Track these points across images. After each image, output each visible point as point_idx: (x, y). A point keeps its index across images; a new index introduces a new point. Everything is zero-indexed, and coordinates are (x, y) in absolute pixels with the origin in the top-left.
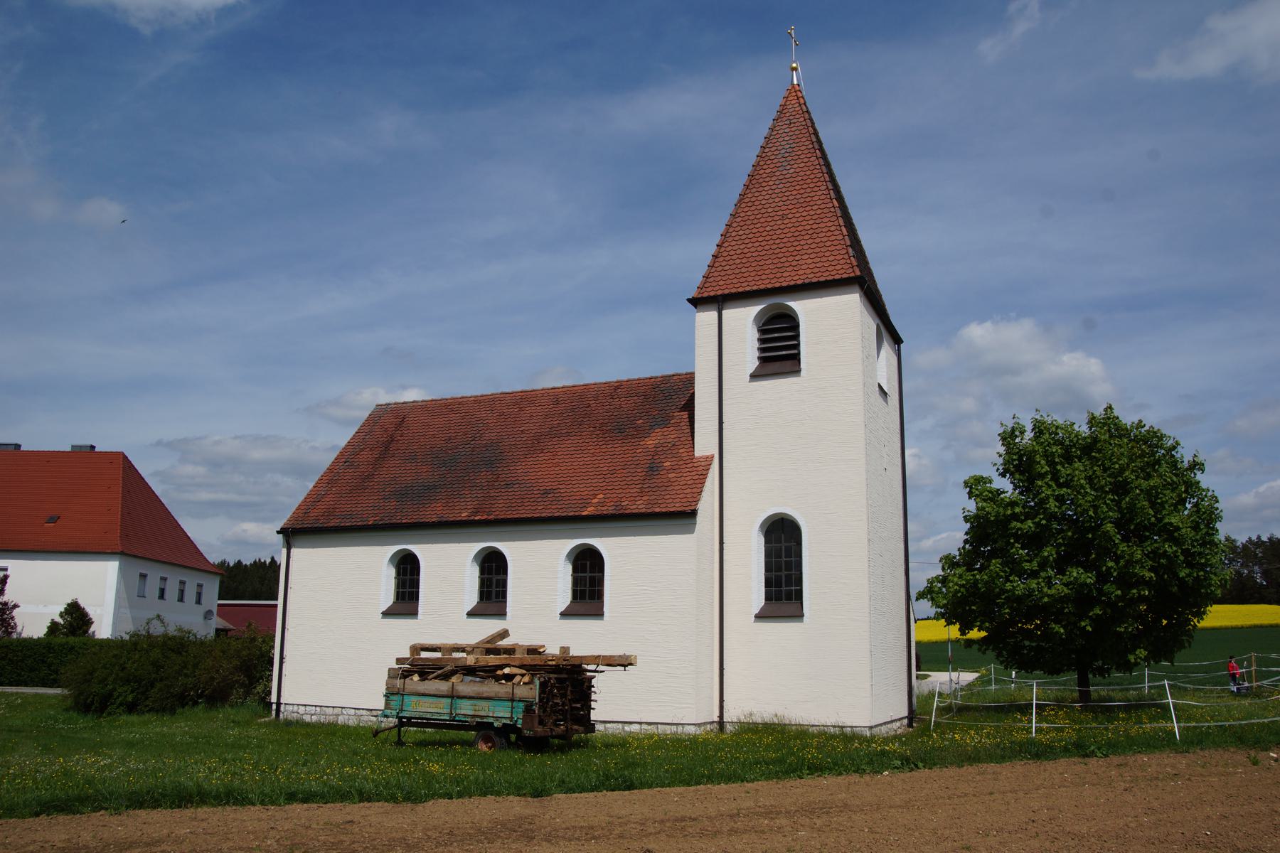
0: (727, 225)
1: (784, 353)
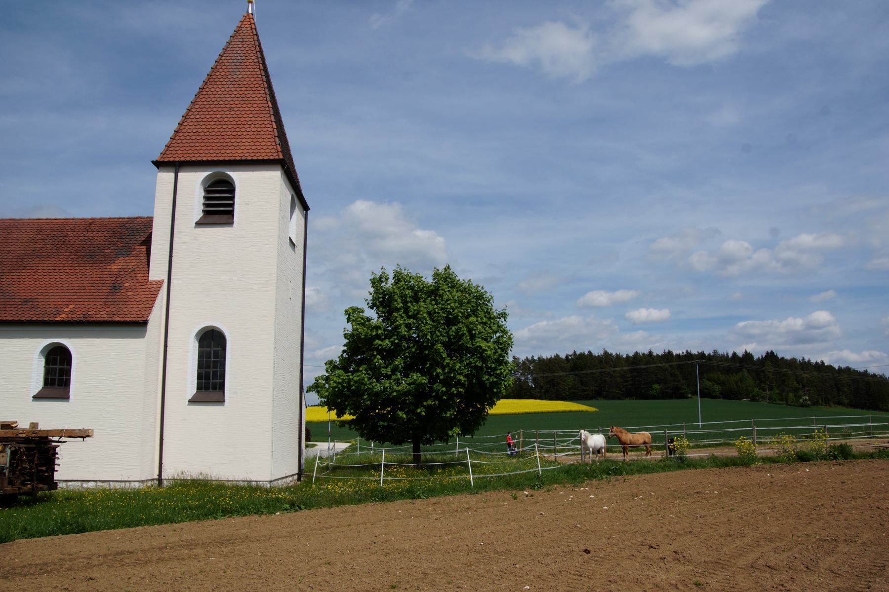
0: (187, 109)
1: (222, 209)
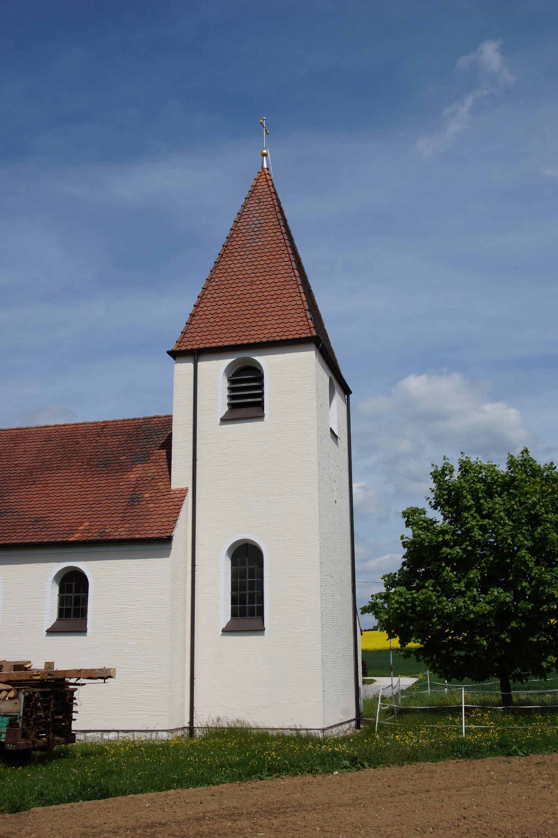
0: (203, 288)
1: (250, 400)
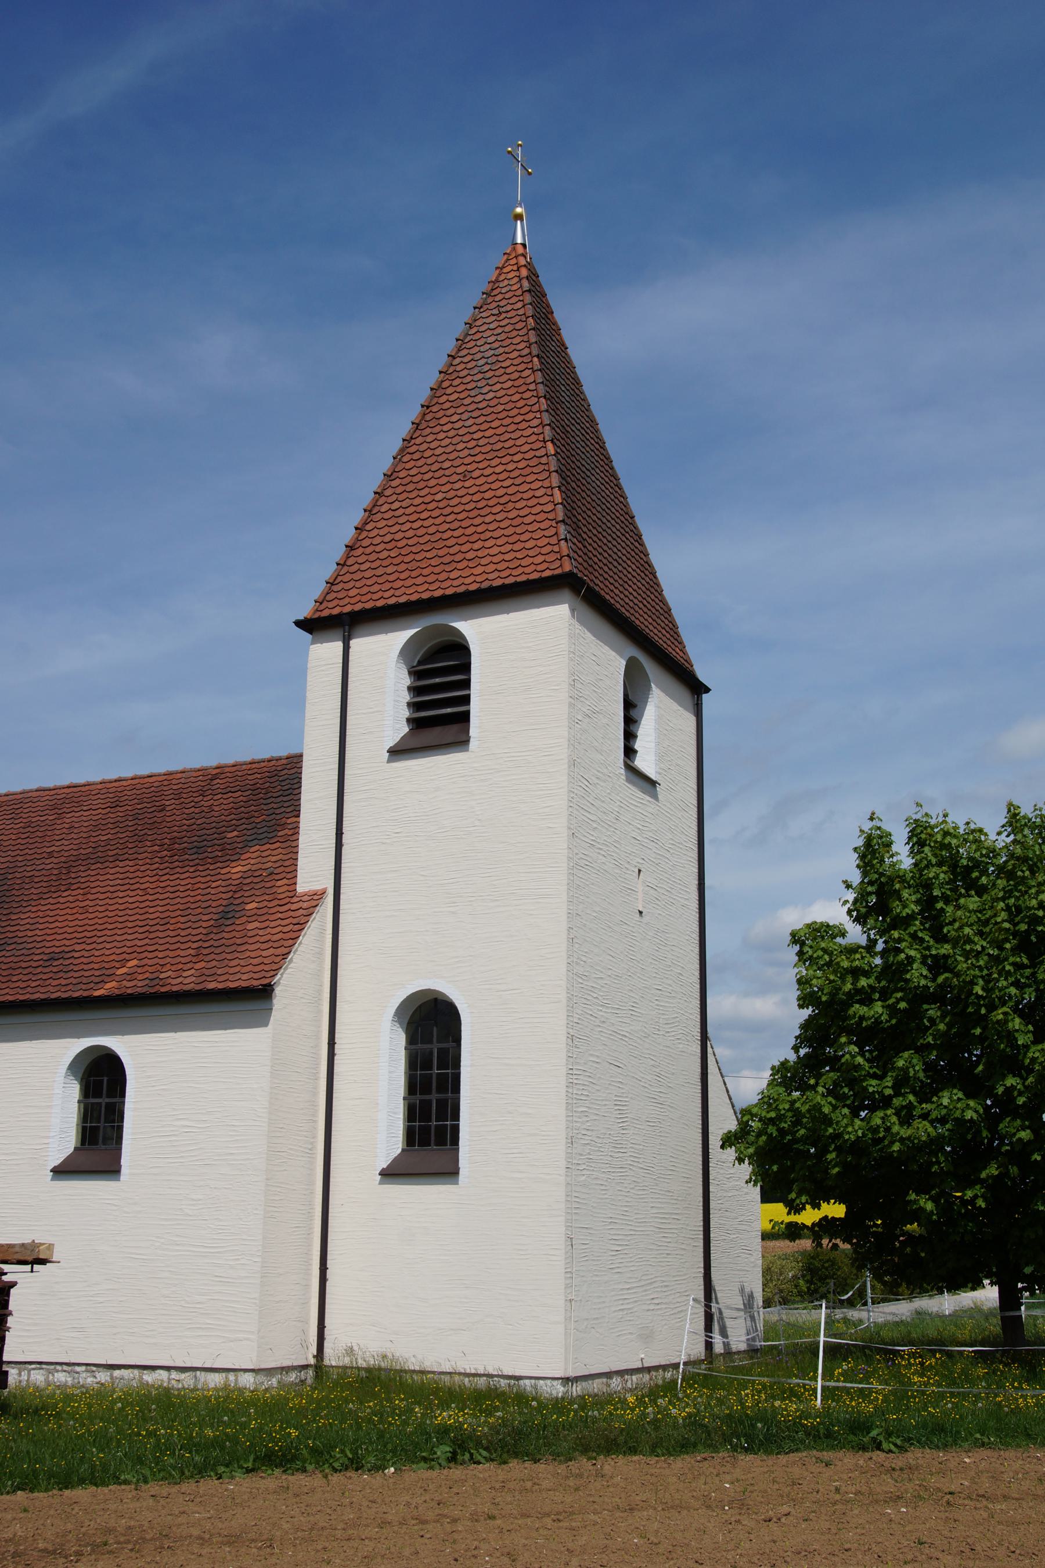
1: (449, 710)
